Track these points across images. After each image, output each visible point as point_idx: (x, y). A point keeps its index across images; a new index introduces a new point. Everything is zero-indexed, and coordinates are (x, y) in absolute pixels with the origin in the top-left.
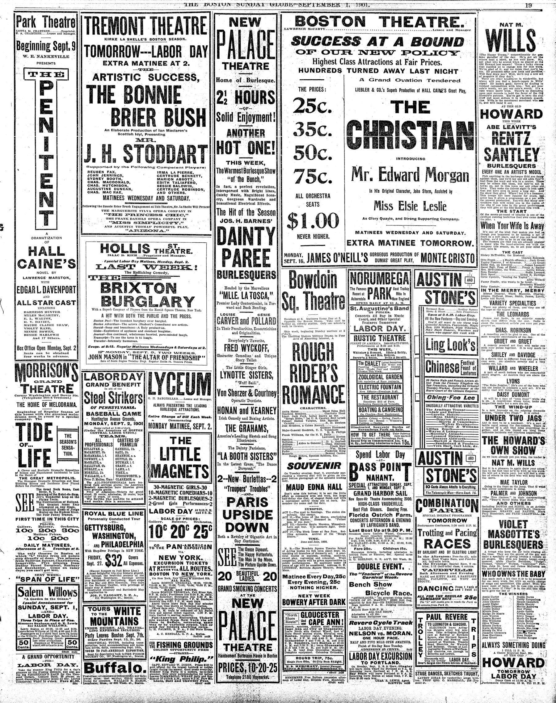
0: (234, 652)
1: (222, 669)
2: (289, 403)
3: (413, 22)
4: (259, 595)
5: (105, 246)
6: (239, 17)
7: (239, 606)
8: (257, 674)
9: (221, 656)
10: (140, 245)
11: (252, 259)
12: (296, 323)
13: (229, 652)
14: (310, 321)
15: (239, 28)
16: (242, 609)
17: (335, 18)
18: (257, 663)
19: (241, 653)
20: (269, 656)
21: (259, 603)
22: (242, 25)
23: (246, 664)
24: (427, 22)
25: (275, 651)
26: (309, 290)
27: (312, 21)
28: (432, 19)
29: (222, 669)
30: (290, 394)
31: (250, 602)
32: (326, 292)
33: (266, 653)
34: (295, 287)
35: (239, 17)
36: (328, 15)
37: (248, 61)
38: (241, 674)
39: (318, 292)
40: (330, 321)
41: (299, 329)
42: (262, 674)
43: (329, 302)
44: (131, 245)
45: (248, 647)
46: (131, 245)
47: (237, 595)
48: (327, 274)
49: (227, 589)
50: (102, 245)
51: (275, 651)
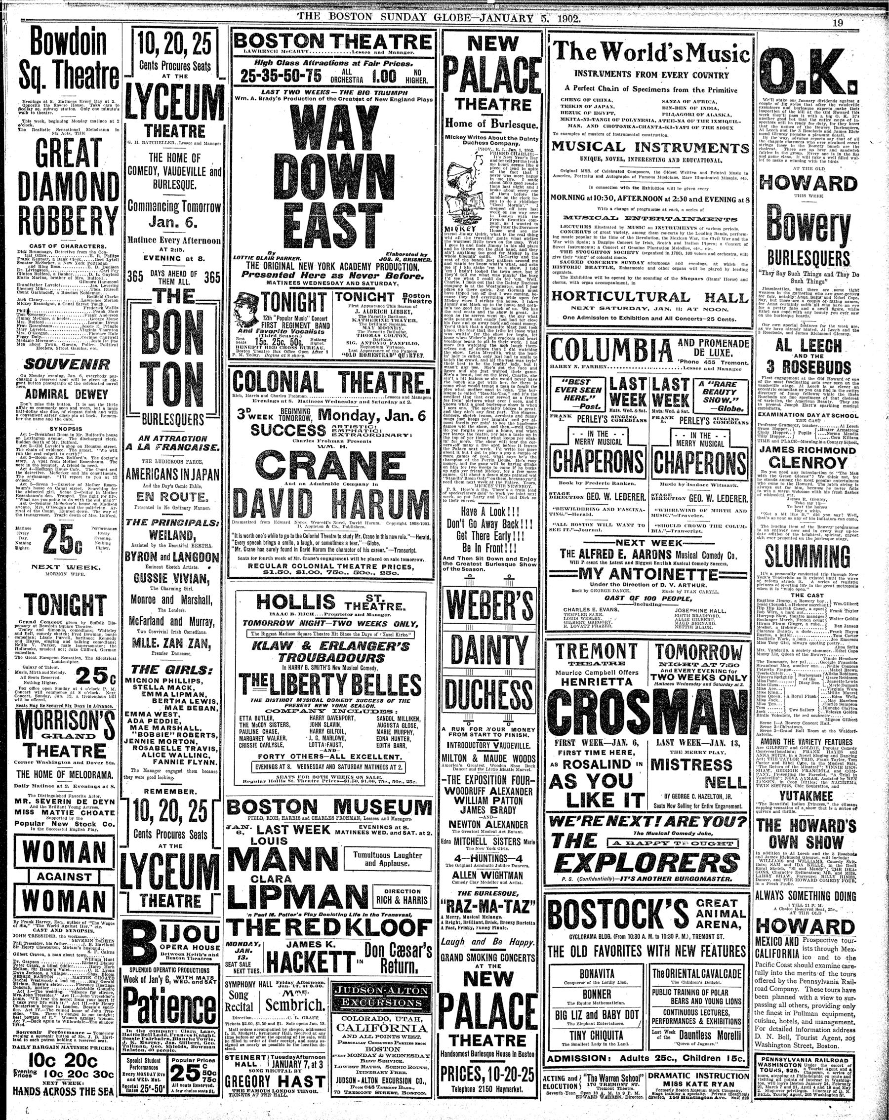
0: (466, 1048)
1: (446, 1077)
2: (28, 233)
3: (372, 42)
4: (507, 967)
5: (263, 598)
6: (484, 35)
7: (475, 984)
8: (502, 1083)
9: (445, 1054)
10: (319, 596)
11: (62, 152)
12: (42, 108)
13: (458, 1048)
14: (62, 105)
15: (484, 52)
16: (479, 989)
17: (286, 37)
18: (502, 1066)
19: (476, 1049)
20: (521, 1054)
21: (506, 978)
22: (487, 49)
23: (485, 1067)
24: (390, 42)
25: (530, 1047)
26: (61, 57)
27: (257, 40)
28: (396, 38)
29: (446, 1077)
30: (31, 220)
31: (492, 977)
32: (89, 61)
33: (517, 1049)
34: (39, 53)
35: (484, 35)
36: (277, 32)
37: (497, 96)
38: (474, 1084)
39: (77, 61)
40: (96, 105)
41: (46, 117)
42: (511, 1084)
43: (92, 76)
44: (305, 596)
45: (488, 1040)
46: (305, 596)
47: (471, 967)
48: (90, 32)
49: (458, 958)
50: (259, 596)
51: (530, 1047)
